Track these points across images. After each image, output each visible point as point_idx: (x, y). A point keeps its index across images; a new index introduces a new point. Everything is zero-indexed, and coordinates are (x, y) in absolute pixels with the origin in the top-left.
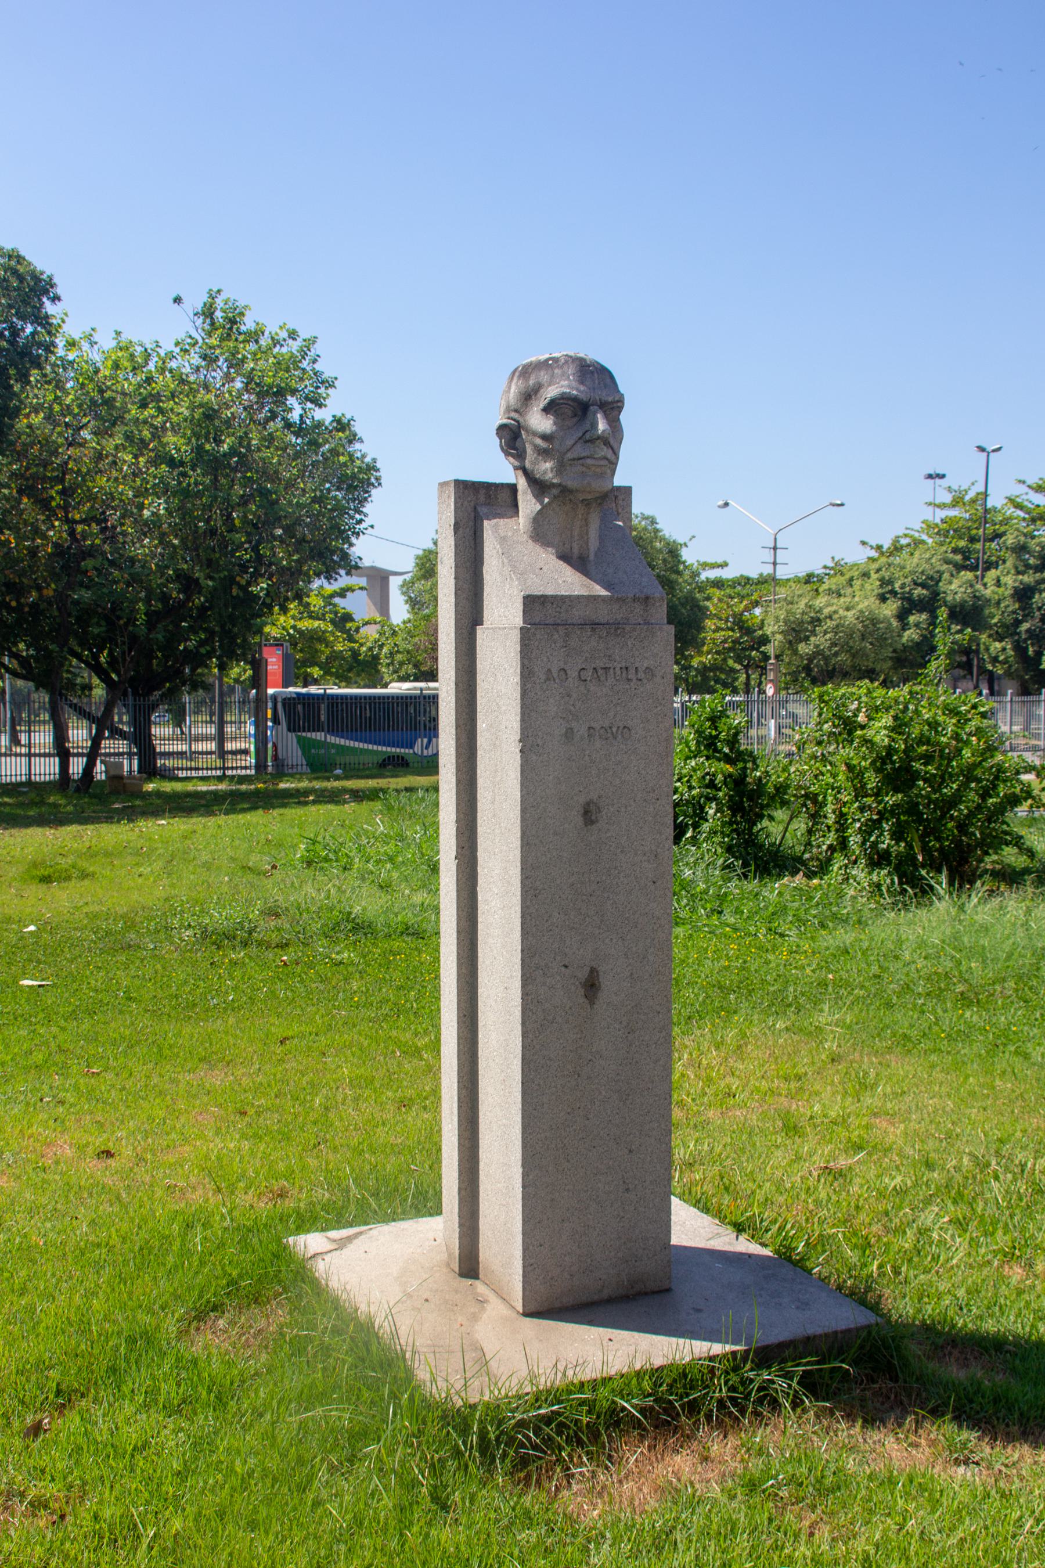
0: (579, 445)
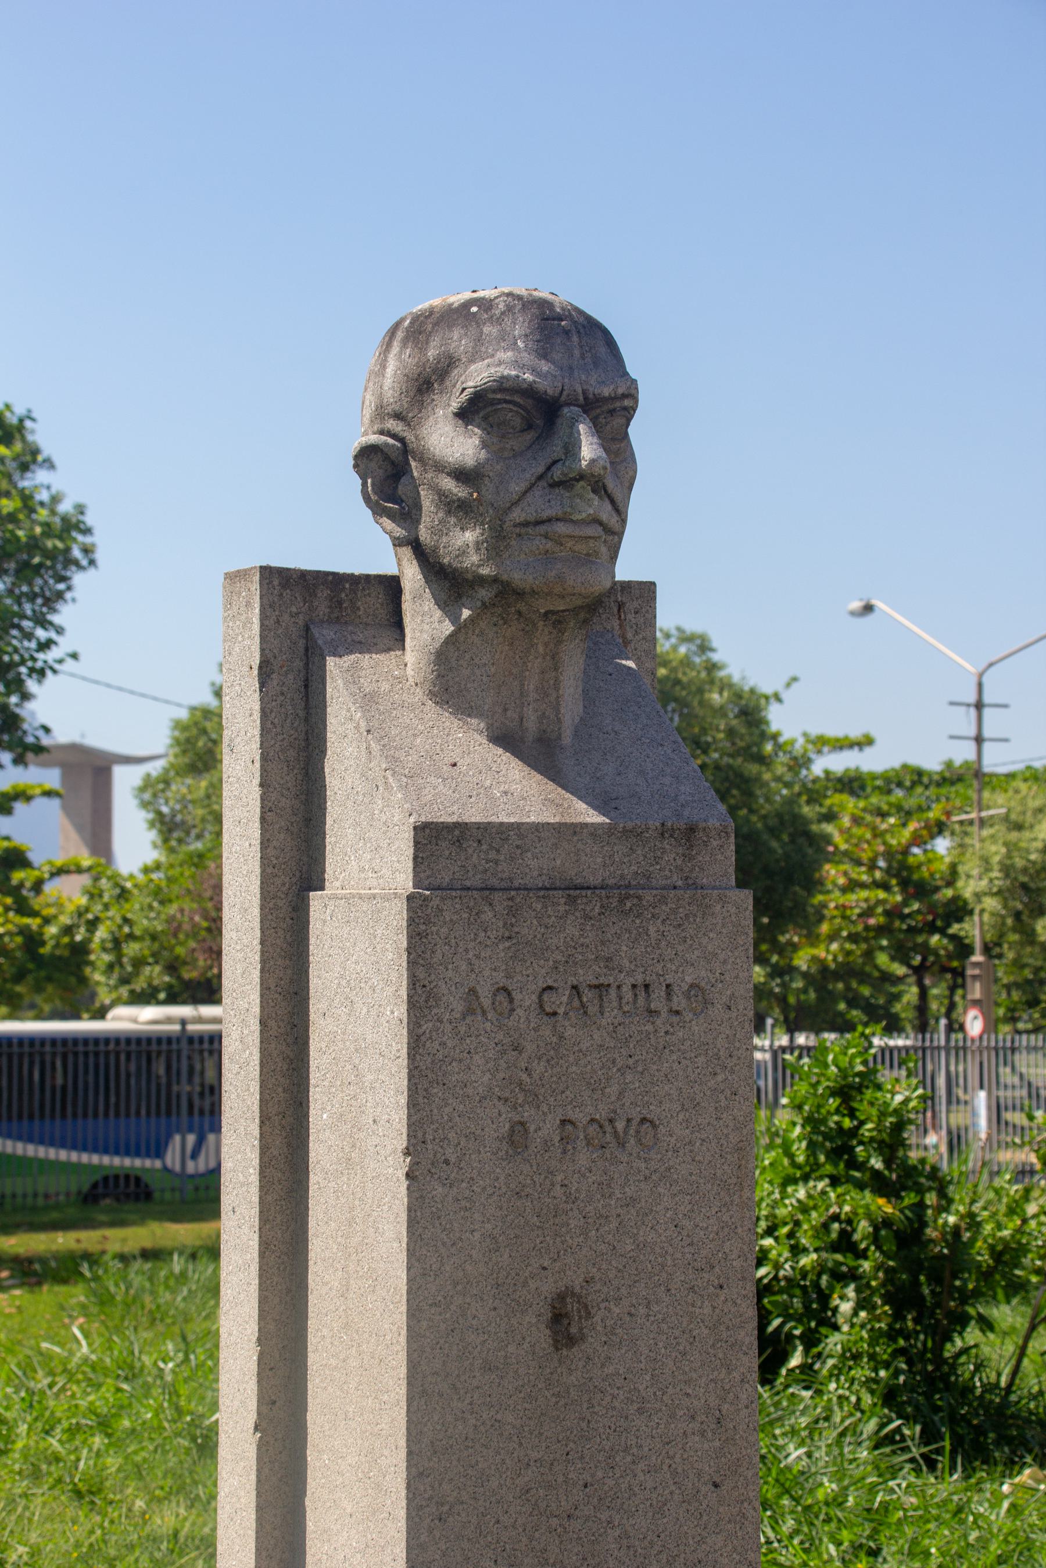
0: (537, 492)
